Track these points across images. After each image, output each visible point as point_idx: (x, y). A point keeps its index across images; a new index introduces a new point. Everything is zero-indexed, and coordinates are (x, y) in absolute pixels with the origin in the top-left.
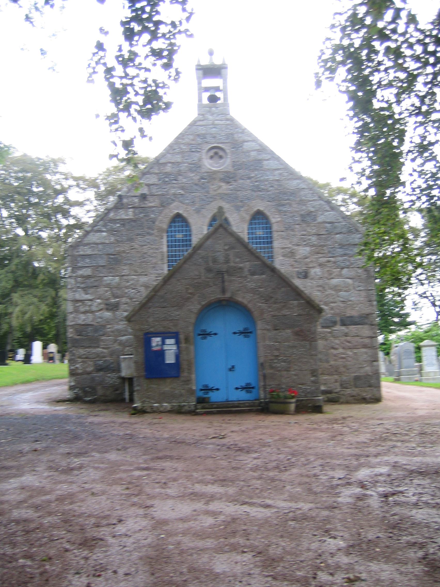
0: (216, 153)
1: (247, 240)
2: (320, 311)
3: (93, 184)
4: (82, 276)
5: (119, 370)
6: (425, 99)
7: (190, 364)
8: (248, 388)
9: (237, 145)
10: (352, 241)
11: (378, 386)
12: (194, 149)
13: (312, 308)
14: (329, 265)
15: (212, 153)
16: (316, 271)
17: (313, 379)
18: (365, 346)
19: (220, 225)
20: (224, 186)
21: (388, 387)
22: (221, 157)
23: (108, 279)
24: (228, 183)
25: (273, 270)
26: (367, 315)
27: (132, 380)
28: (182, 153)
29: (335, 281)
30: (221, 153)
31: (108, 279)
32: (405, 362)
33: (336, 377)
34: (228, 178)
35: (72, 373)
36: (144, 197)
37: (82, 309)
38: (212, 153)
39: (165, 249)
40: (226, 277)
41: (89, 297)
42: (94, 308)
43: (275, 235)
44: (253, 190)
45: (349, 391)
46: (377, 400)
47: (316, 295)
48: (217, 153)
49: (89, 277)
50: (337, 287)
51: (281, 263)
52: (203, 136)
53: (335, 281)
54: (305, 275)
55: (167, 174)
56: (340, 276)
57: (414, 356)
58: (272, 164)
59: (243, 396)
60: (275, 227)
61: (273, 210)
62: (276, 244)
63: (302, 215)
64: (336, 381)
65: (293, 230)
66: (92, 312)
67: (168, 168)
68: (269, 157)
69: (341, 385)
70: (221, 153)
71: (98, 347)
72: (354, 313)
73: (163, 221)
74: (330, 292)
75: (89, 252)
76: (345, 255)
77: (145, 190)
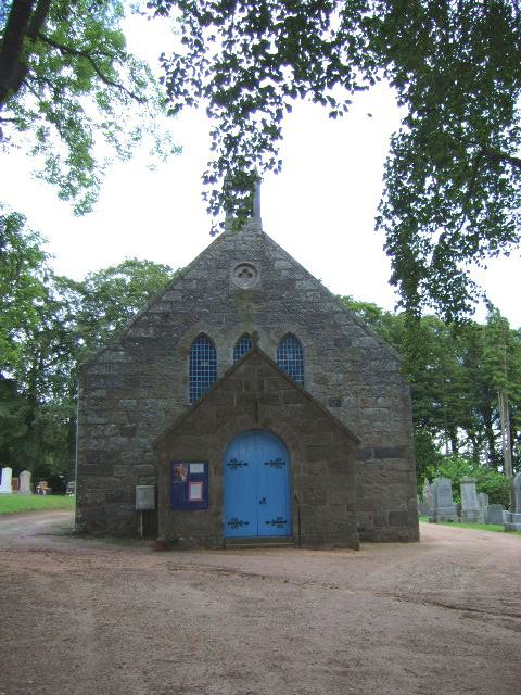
0: (245, 271)
1: (276, 360)
2: (358, 442)
3: (80, 288)
4: (95, 398)
5: (133, 500)
6: (71, 69)
7: (221, 497)
8: (279, 522)
9: (267, 264)
10: (388, 368)
11: (416, 525)
12: (223, 266)
13: (348, 437)
14: (364, 393)
15: (240, 270)
16: (349, 399)
17: (349, 513)
18: (400, 481)
19: (247, 343)
20: (254, 306)
21: (425, 527)
22: (250, 275)
23: (124, 402)
24: (257, 302)
25: (309, 398)
26: (403, 448)
27: (145, 510)
28: (209, 269)
29: (370, 411)
30: (250, 271)
31: (124, 402)
32: (441, 500)
33: (370, 513)
34: (256, 297)
35: (79, 505)
36: (166, 316)
37: (93, 434)
38: (240, 270)
39: (188, 372)
40: (259, 404)
41: (102, 420)
42: (107, 433)
43: (306, 360)
44: (284, 312)
45: (384, 529)
46: (416, 538)
47: (351, 425)
48: (246, 270)
49: (102, 399)
50: (376, 415)
51: (311, 387)
52: (232, 253)
53: (370, 411)
54: (338, 403)
55: (192, 291)
56: (375, 404)
57: (451, 493)
58: (306, 284)
59: (274, 531)
60: (306, 352)
61: (305, 333)
62: (308, 369)
63: (336, 340)
64: (370, 518)
65: (326, 355)
66: (106, 437)
67: (194, 285)
68: (301, 276)
69: (375, 523)
70: (250, 271)
71: (111, 475)
72: (390, 445)
73: (186, 340)
74: (363, 421)
75: (104, 372)
76: (381, 383)
77: (168, 308)
